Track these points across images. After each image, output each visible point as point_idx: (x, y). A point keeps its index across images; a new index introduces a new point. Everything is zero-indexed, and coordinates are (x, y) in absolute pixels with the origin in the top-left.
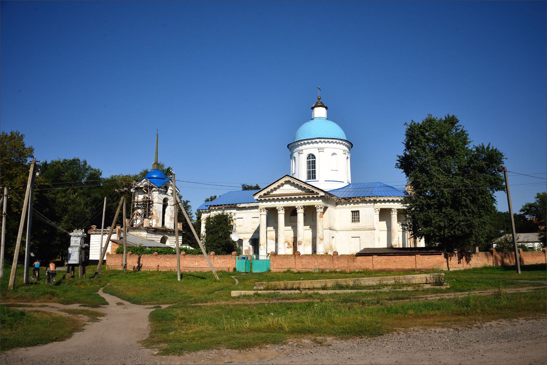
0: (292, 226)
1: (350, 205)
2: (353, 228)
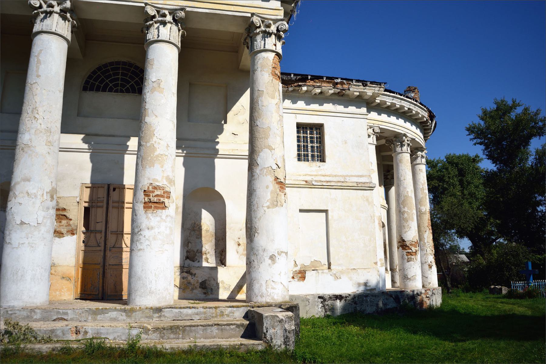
0: (87, 135)
1: (294, 102)
2: (308, 178)
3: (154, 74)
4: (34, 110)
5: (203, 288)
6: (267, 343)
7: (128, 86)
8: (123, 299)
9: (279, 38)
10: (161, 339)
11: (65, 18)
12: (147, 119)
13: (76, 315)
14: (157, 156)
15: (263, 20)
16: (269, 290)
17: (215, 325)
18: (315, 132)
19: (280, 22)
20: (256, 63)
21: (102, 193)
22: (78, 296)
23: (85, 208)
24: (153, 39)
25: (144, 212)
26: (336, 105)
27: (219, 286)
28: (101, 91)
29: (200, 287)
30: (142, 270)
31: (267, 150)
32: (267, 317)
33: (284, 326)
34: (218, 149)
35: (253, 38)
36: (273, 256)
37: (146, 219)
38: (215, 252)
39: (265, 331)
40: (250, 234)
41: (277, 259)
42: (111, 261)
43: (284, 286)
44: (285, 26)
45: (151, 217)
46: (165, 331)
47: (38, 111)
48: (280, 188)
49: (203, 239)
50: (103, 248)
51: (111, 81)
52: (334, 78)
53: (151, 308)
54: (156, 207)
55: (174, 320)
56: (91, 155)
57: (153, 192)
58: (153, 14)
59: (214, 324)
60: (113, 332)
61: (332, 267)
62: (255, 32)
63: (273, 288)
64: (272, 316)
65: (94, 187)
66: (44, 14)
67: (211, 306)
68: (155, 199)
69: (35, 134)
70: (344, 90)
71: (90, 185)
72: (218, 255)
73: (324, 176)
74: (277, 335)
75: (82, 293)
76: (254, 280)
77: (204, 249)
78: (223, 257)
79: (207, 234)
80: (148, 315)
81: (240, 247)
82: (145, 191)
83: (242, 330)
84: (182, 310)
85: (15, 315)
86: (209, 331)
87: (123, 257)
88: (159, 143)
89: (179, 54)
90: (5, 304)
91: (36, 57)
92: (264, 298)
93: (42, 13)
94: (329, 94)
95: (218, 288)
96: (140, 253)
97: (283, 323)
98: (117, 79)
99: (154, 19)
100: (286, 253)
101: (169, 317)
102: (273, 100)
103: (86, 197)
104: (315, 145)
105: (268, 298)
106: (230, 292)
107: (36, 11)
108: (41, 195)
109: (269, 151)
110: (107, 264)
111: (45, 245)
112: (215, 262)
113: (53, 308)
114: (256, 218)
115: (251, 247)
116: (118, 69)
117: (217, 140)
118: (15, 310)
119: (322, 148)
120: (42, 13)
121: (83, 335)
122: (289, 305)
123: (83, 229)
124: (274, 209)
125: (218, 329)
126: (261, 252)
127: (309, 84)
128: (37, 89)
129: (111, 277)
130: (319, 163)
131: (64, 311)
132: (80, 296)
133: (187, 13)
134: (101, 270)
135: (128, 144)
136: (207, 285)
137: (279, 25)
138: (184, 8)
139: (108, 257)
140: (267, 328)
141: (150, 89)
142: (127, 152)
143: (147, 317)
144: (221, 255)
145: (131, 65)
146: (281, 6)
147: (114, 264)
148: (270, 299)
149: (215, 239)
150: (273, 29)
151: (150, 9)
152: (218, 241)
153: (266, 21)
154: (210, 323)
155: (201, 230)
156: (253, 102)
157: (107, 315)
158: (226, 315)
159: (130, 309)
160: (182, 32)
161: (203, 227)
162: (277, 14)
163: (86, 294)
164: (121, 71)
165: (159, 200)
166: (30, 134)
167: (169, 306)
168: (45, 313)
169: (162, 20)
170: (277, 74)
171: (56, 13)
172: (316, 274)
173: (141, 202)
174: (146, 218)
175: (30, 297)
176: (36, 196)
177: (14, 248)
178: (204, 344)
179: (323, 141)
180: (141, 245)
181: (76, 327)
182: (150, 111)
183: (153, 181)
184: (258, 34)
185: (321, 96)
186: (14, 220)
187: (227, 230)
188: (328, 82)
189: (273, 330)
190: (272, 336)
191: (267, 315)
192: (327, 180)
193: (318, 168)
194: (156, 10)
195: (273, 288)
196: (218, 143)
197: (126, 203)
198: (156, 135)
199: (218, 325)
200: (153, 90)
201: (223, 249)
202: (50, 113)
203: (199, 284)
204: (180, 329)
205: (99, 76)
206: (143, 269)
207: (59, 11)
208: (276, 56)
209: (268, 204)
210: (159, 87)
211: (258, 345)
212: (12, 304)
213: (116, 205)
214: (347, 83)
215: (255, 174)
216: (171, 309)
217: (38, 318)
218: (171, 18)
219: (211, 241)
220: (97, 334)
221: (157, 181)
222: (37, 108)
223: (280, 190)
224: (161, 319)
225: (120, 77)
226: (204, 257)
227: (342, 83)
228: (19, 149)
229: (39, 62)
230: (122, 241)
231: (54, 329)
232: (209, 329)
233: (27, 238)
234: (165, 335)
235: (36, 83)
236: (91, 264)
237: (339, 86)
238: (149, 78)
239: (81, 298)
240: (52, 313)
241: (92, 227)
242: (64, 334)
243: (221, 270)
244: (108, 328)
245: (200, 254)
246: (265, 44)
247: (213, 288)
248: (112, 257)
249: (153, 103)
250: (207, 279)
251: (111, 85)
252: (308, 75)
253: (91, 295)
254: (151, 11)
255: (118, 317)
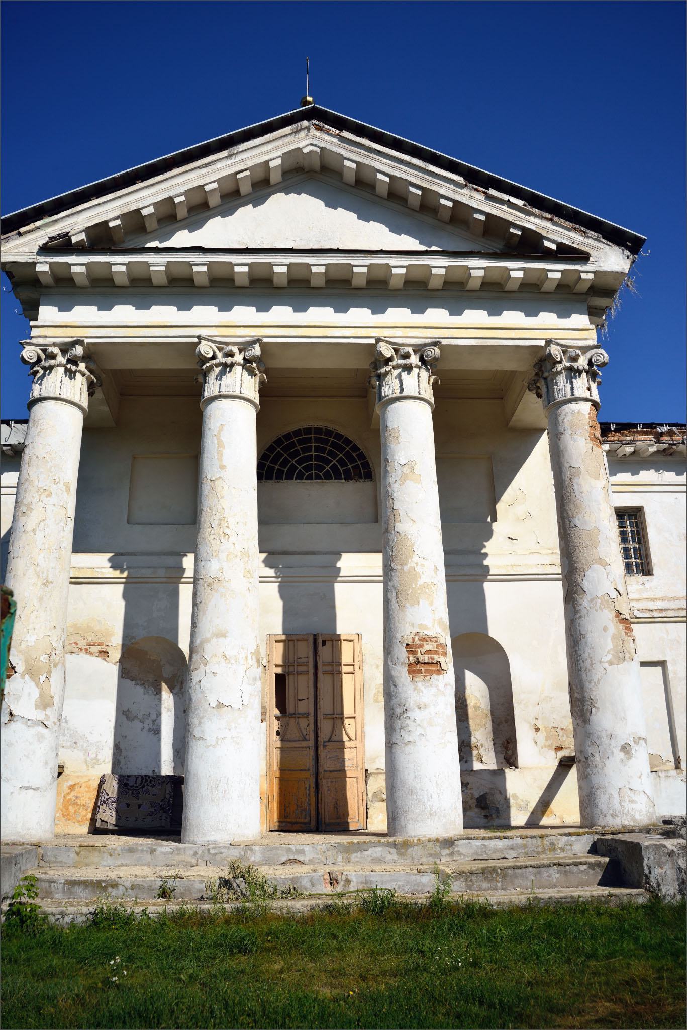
3: (402, 452)
4: (222, 522)
5: (483, 808)
6: (652, 892)
7: (327, 468)
8: (351, 829)
9: (593, 375)
10: (468, 891)
11: (251, 373)
12: (399, 527)
13: (318, 854)
14: (422, 587)
15: (565, 349)
16: (625, 804)
17: (555, 864)
18: (628, 521)
19: (594, 351)
20: (561, 422)
21: (304, 650)
22: (276, 826)
23: (277, 676)
24: (394, 396)
25: (409, 680)
26: (661, 471)
27: (509, 803)
28: (286, 479)
29: (477, 806)
30: (415, 777)
31: (597, 567)
32: (647, 847)
33: (677, 863)
34: (488, 567)
35: (549, 379)
36: (626, 746)
37: (414, 691)
38: (494, 745)
39: (647, 871)
40: (582, 711)
41: (633, 751)
42: (327, 765)
43: (648, 796)
44: (603, 356)
45: (423, 688)
46: (473, 878)
47: (228, 523)
48: (626, 629)
49: (471, 722)
50: (313, 743)
51: (299, 462)
52: (655, 424)
53: (437, 840)
54: (427, 671)
55: (474, 860)
56: (279, 587)
57: (421, 646)
58: (389, 356)
59: (553, 863)
60: (392, 880)
61: (683, 765)
62: (554, 370)
63: (632, 801)
64: (655, 845)
65: (290, 640)
66: (220, 368)
67: (533, 834)
68: (426, 659)
69: (227, 560)
70: (675, 444)
71: (283, 637)
72: (499, 749)
73: (652, 600)
74: (667, 877)
75: (281, 820)
76: (598, 789)
77: (473, 740)
78: (510, 753)
79: (477, 713)
80: (432, 852)
81: (538, 733)
82: (407, 645)
83: (598, 873)
84: (487, 843)
85: (221, 856)
86: (545, 875)
87: (346, 757)
88: (422, 565)
89: (432, 413)
90: (200, 839)
91: (215, 437)
92: (619, 818)
93: (217, 365)
94: (648, 453)
95: (508, 807)
96: (408, 749)
97: (675, 857)
98: (309, 458)
99: (390, 363)
100: (645, 740)
101: (466, 855)
102: (597, 481)
103: (278, 657)
104: (631, 545)
105: (624, 818)
106: (529, 814)
107: (208, 365)
108: (244, 658)
109: (602, 568)
110: (321, 770)
111: (254, 740)
112: (494, 761)
113: (281, 842)
114: (590, 682)
115: (586, 732)
116: (309, 440)
117: (483, 551)
118: (220, 847)
119: (643, 550)
120: (217, 365)
121: (344, 885)
122: (662, 829)
123: (277, 712)
124: (620, 666)
125: (559, 872)
126: (605, 740)
127: (612, 439)
128: (223, 488)
129: (329, 792)
130: (641, 578)
131: (298, 847)
132: (279, 826)
133: (443, 348)
134: (313, 780)
135: (338, 565)
136: (488, 802)
137: (592, 355)
138: (438, 342)
139: (322, 759)
140: (650, 867)
141: (397, 477)
142: (339, 579)
143: (431, 855)
144: (506, 748)
145: (329, 433)
146: (591, 324)
147: (331, 769)
148: (629, 820)
149: (493, 721)
150: (582, 362)
151: (385, 347)
152: (498, 725)
153: (570, 350)
154: (546, 862)
155: (466, 706)
156: (563, 487)
157: (366, 853)
158: (560, 849)
159: (403, 842)
160: (434, 379)
161: (468, 702)
162: (585, 337)
163: (289, 822)
164: (313, 444)
165: (433, 659)
166: (219, 560)
167: (465, 837)
168: (268, 851)
169: (405, 364)
170: (597, 438)
171: (239, 364)
172: (655, 778)
173: (402, 664)
174: (415, 689)
175: (239, 826)
176: (237, 661)
177: (209, 746)
178: (550, 895)
179: (644, 538)
180: (409, 735)
181: (329, 873)
182: (402, 513)
183: (420, 628)
184: (560, 373)
185: (634, 458)
186: (206, 700)
187: (515, 705)
188: (646, 433)
189: (660, 870)
190: (659, 879)
191: (647, 844)
192: (660, 608)
193: (642, 587)
194: (393, 348)
195: (632, 801)
196: (486, 555)
197: (344, 665)
198: (417, 552)
199: (559, 864)
200: (403, 479)
201: (510, 738)
202: (246, 524)
203: (474, 801)
204: (497, 873)
205: (279, 455)
206: (416, 774)
207: (242, 362)
208: (593, 407)
209: (609, 657)
210: (413, 473)
211: (638, 896)
212: (212, 839)
213: (329, 668)
214: (680, 432)
215: (580, 607)
216: (468, 841)
217: (257, 861)
218: (418, 359)
219: (485, 725)
220: (366, 883)
221: (426, 627)
222: (226, 519)
223: (625, 632)
224: (454, 859)
225: (313, 453)
226: (475, 753)
227: (670, 433)
228: (203, 585)
229: (221, 444)
230: (342, 733)
231: (297, 877)
232: (545, 872)
233: (230, 730)
234: (474, 884)
235: (220, 478)
236: (293, 770)
237: (666, 438)
238: (394, 460)
239: (280, 829)
240: (279, 852)
241: (290, 708)
242: (313, 885)
243: (510, 774)
244: (382, 873)
245: (467, 748)
246: (572, 389)
247: (500, 807)
248: (329, 758)
249: (407, 499)
250: (488, 791)
251: (300, 468)
252: (610, 424)
253: (296, 823)
254: (386, 351)
255: (384, 856)
